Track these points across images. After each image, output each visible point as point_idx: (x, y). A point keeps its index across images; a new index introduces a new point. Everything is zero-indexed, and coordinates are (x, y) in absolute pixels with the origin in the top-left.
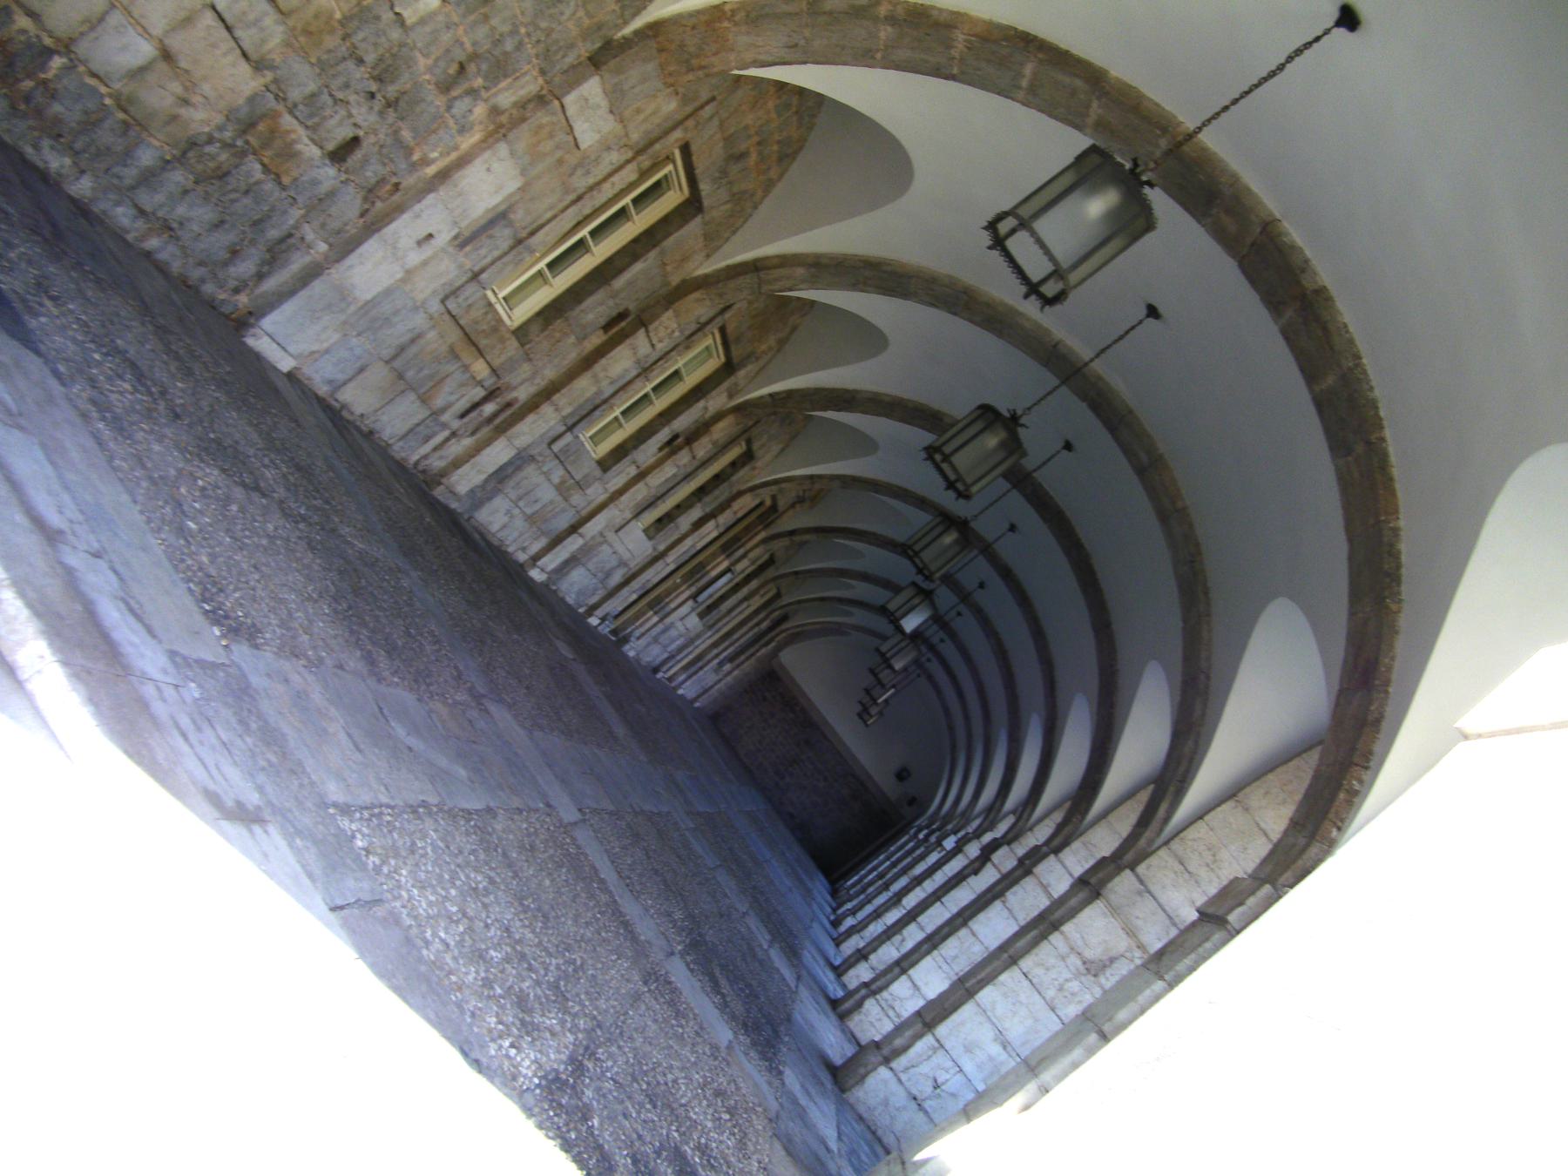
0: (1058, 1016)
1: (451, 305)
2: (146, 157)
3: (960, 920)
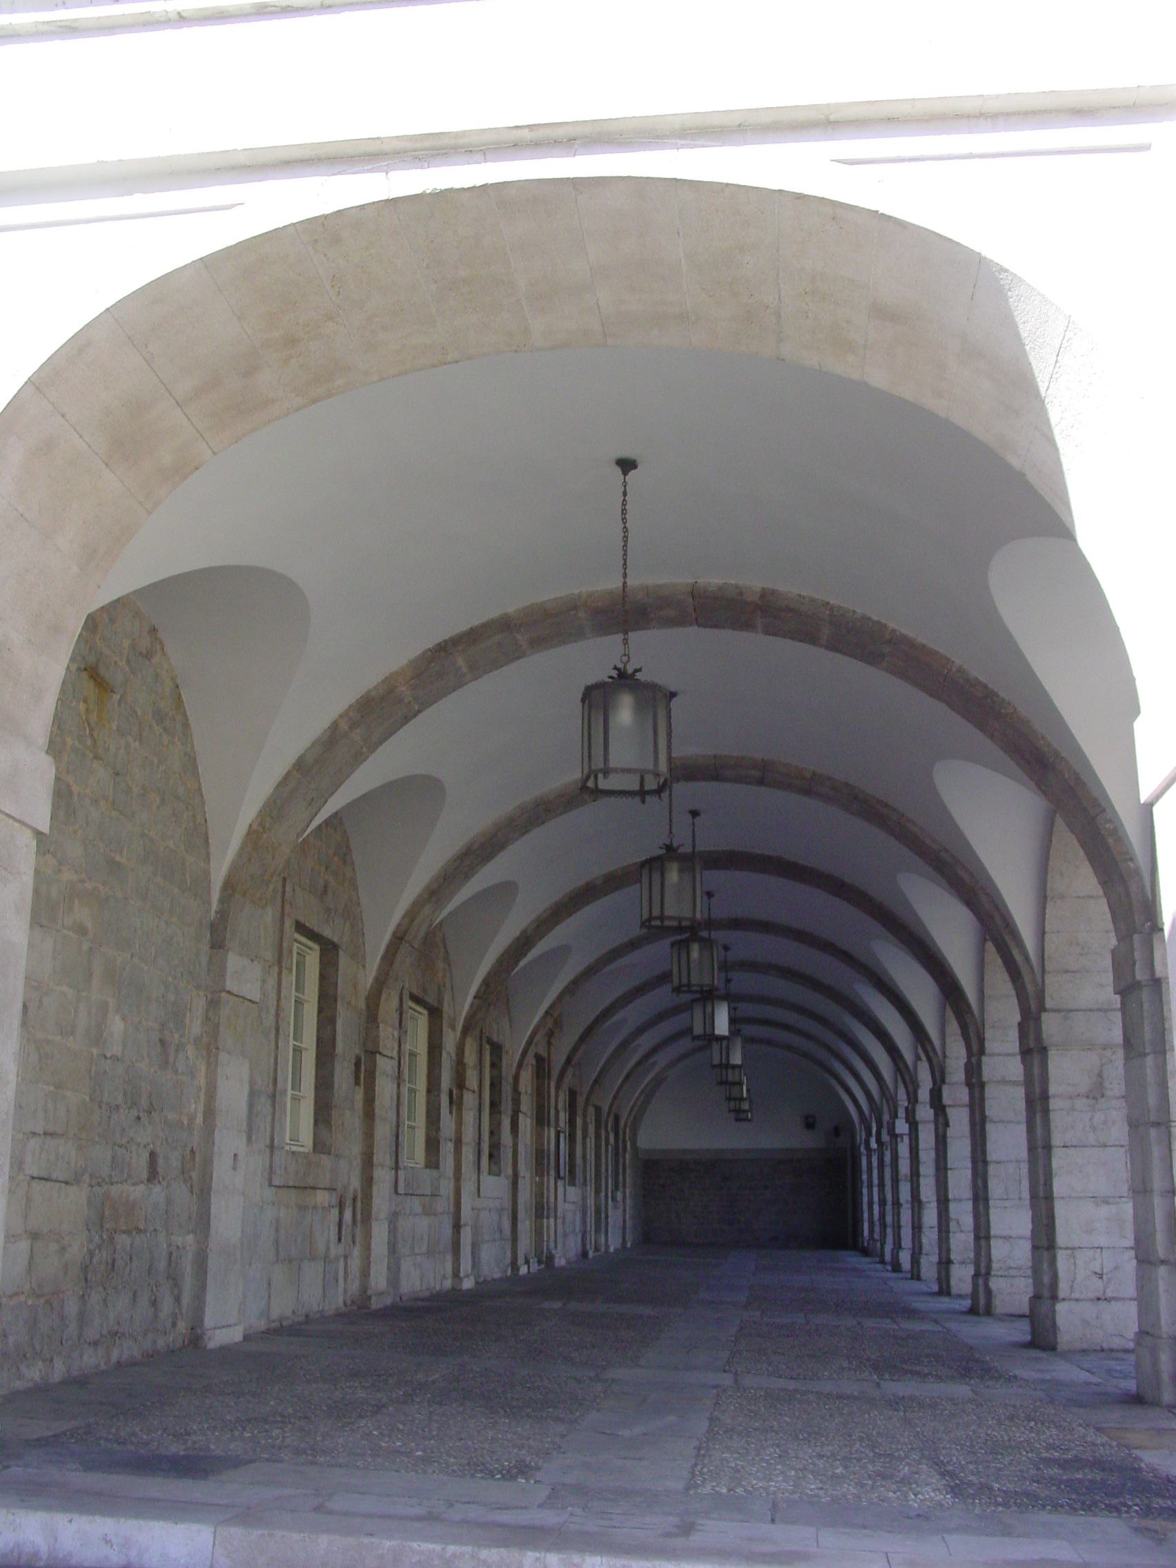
0: (1111, 1146)
1: (276, 1182)
2: (72, 1308)
3: (980, 1165)
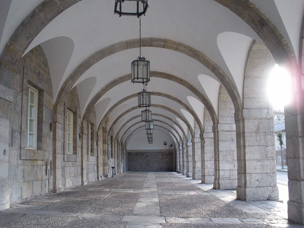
0: (261, 146)
